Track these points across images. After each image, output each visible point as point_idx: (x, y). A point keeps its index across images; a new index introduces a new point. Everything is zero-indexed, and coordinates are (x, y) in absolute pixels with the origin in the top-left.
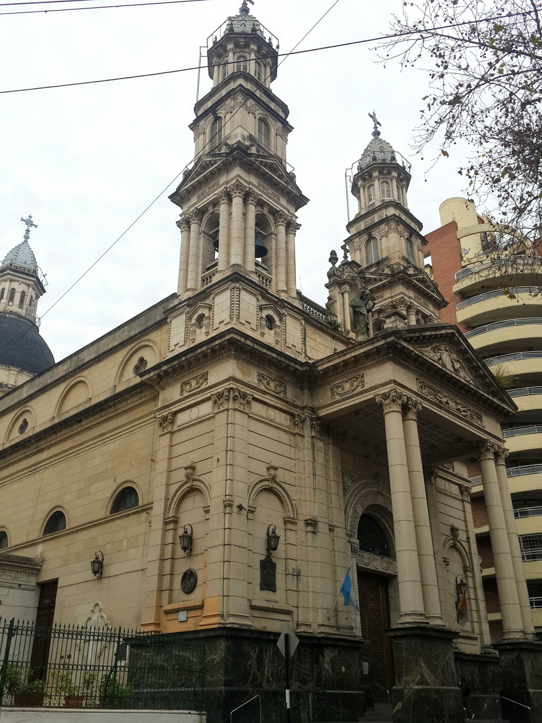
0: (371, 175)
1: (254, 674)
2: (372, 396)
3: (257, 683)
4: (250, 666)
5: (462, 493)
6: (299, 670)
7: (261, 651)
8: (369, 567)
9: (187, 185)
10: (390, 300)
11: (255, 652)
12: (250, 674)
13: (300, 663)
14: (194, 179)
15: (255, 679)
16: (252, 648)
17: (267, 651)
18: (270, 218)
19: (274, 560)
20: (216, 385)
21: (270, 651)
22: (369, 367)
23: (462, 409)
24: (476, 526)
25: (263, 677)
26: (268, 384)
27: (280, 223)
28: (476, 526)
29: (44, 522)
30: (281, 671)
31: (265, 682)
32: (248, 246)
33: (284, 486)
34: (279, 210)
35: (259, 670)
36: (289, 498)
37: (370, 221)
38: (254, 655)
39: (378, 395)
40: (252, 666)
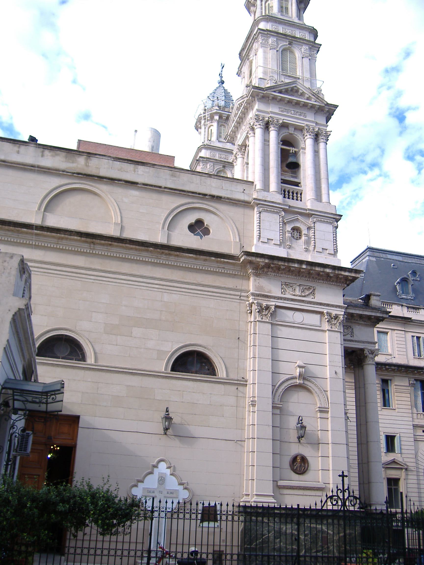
2: (362, 347)
9: (275, 92)
20: (321, 304)
22: (359, 324)
39: (367, 349)
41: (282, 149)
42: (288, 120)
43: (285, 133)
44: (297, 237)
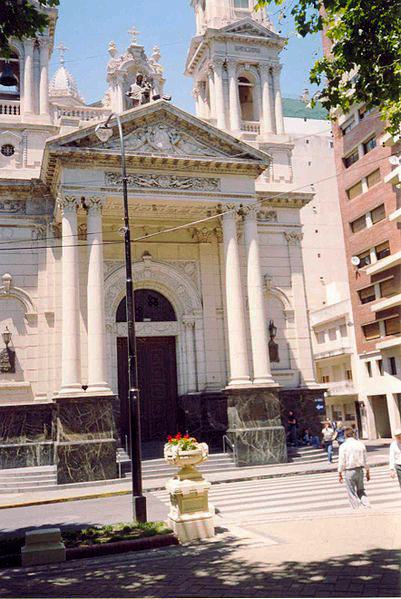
18: (253, 71)
19: (276, 342)
23: (179, 184)
41: (240, 86)
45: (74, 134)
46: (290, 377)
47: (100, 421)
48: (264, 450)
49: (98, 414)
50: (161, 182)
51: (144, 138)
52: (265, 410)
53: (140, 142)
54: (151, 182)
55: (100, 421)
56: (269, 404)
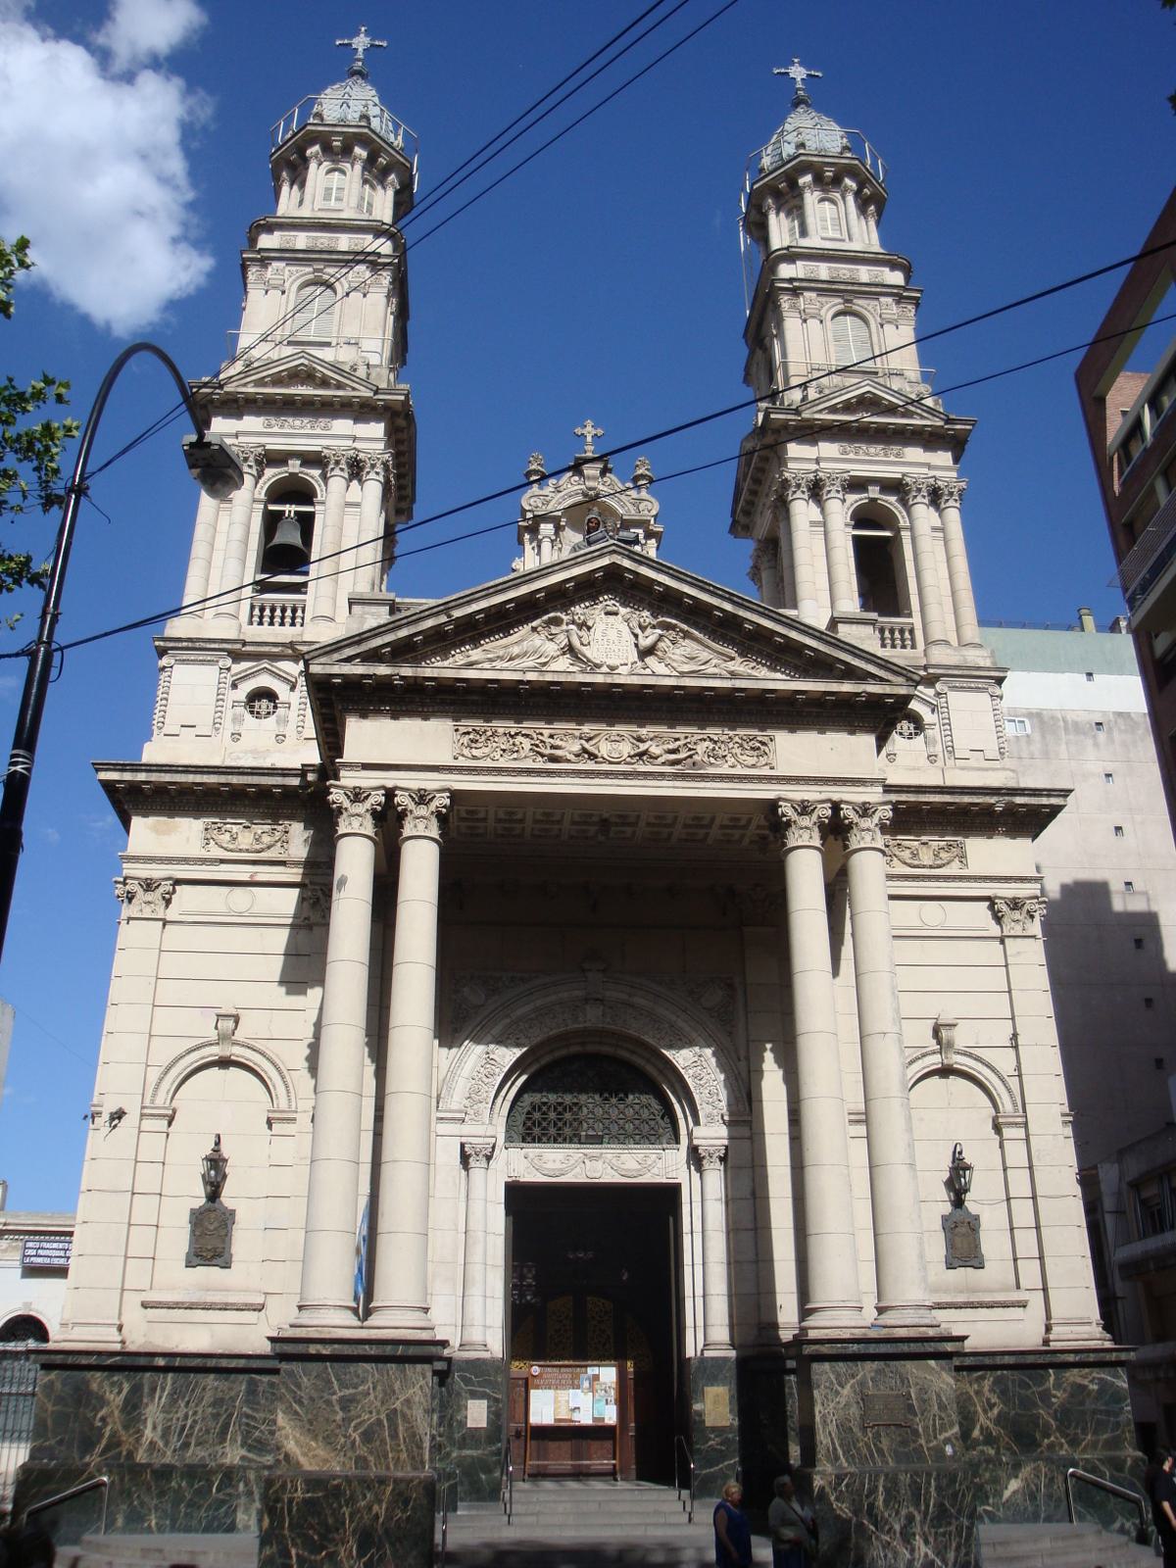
0: (793, 184)
1: (114, 1434)
3: (120, 1453)
4: (103, 1419)
5: (998, 918)
6: (247, 1425)
7: (136, 1390)
8: (601, 1180)
10: (349, 443)
11: (119, 1393)
12: (101, 1436)
13: (252, 1408)
14: (265, 385)
15: (114, 1443)
16: (113, 1384)
17: (153, 1390)
18: (891, 501)
21: (163, 1389)
23: (655, 750)
24: (666, 1197)
25: (138, 1440)
26: (915, 855)
27: (832, 495)
28: (666, 1197)
29: (277, 1055)
30: (192, 1427)
31: (141, 1451)
32: (954, 559)
33: (258, 1045)
34: (899, 476)
35: (126, 1427)
36: (278, 1069)
37: (326, 242)
38: (116, 1399)
40: (109, 1420)
41: (856, 540)
42: (276, 444)
43: (272, 474)
44: (911, 734)
45: (376, 632)
46: (1017, 1312)
47: (392, 1415)
48: (907, 1537)
49: (389, 1393)
50: (604, 749)
51: (562, 640)
52: (910, 1408)
53: (551, 648)
54: (576, 748)
55: (392, 1415)
56: (923, 1390)
